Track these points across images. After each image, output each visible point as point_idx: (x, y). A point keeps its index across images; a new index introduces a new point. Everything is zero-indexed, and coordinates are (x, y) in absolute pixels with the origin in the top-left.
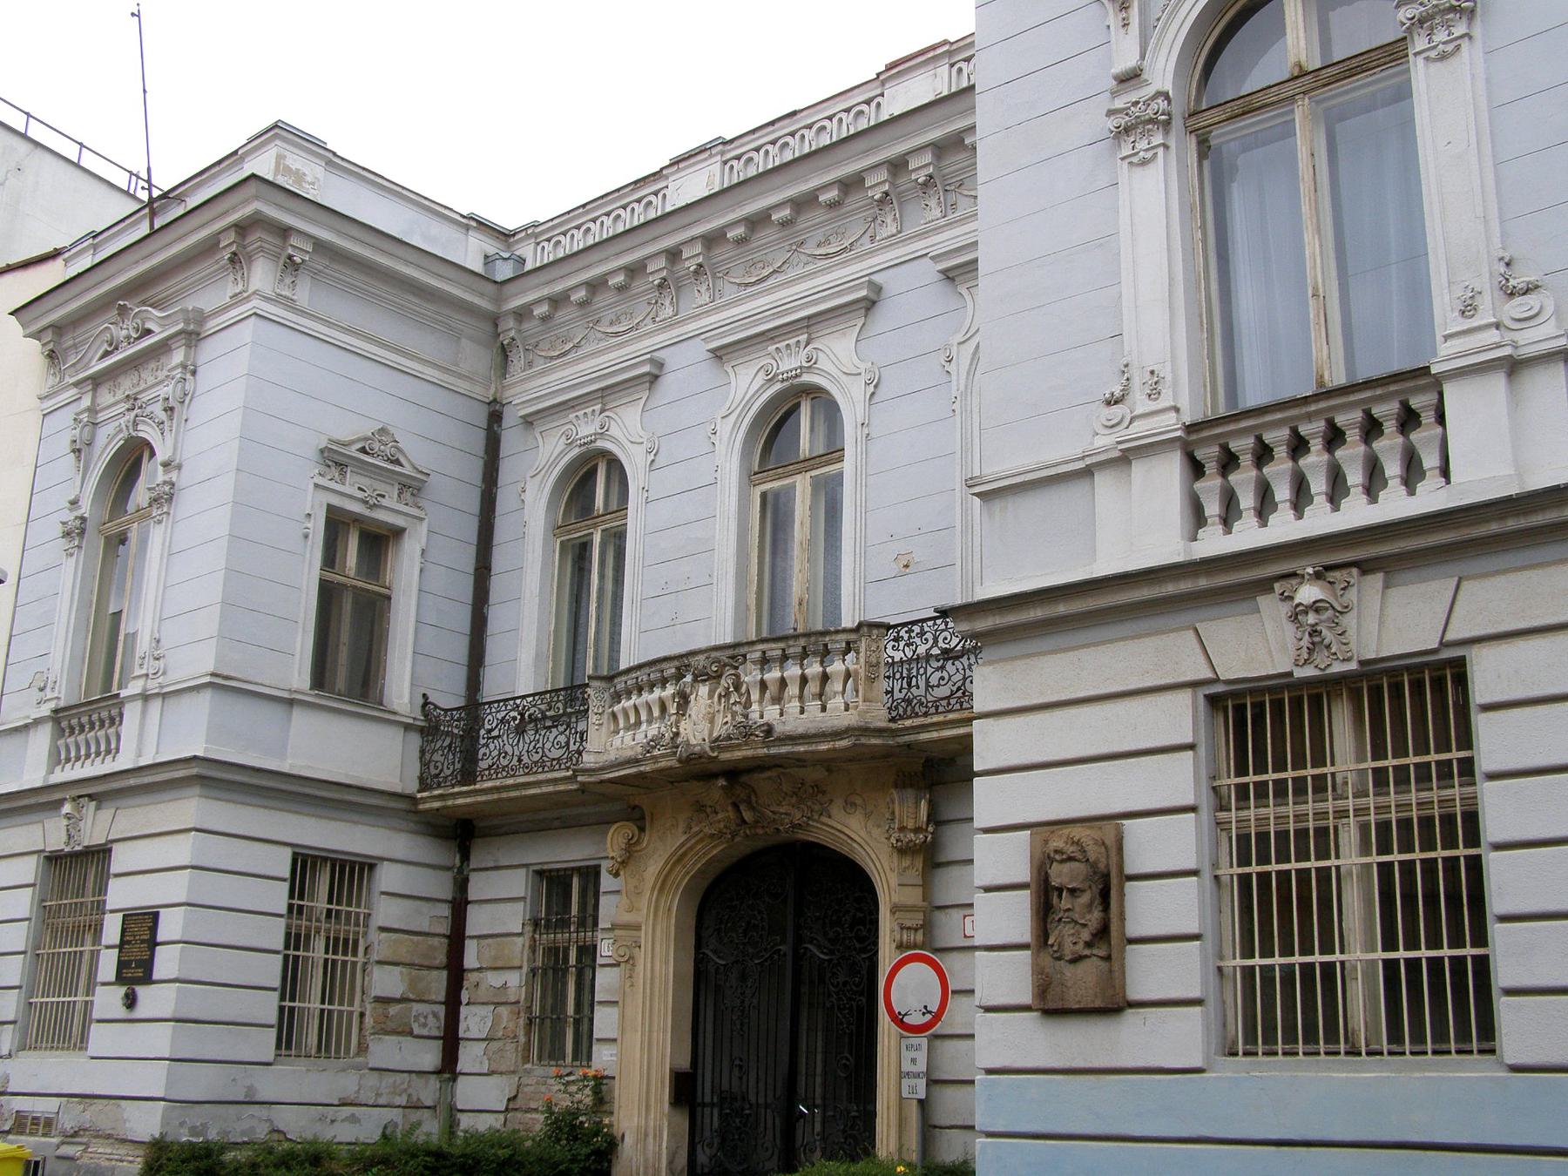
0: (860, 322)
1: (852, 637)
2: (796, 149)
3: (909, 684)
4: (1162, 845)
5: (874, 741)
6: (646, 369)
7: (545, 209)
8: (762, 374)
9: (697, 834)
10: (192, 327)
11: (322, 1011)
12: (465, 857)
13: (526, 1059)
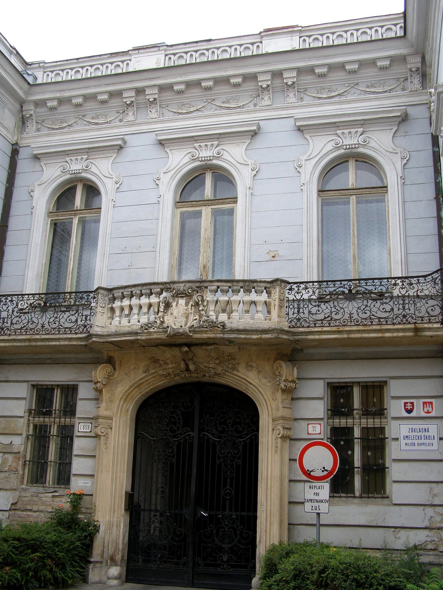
0: (248, 141)
1: (268, 285)
2: (209, 56)
5: (285, 337)
6: (120, 142)
7: (49, 58)
9: (153, 373)
13: (22, 483)
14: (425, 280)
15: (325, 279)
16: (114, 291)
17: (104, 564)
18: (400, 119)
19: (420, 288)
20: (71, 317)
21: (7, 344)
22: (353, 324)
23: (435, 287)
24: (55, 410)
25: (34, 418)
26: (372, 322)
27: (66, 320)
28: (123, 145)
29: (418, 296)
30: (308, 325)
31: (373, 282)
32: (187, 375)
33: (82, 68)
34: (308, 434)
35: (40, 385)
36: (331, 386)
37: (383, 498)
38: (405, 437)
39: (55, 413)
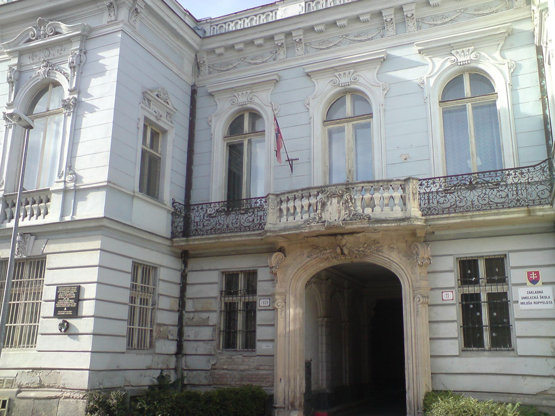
0: (378, 67)
4: (90, 292)
6: (275, 77)
7: (214, 15)
8: (332, 83)
10: (85, 33)
11: (139, 329)
14: (535, 169)
15: (449, 175)
16: (281, 196)
19: (530, 176)
21: (201, 242)
24: (241, 290)
26: (490, 207)
28: (278, 79)
29: (529, 183)
30: (437, 212)
31: (490, 174)
33: (240, 19)
37: (508, 350)
38: (524, 299)
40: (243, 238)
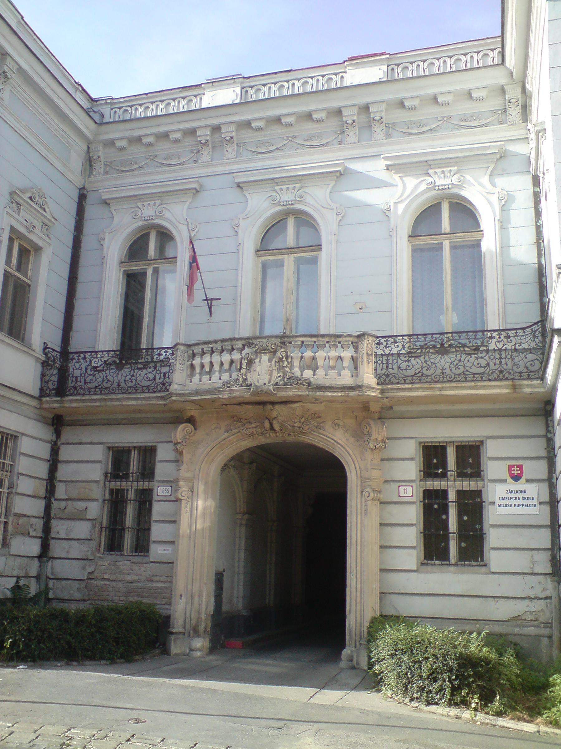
0: (333, 183)
3: (164, 376)
6: (195, 186)
12: (58, 434)
14: (524, 332)
17: (187, 635)
18: (498, 156)
19: (518, 341)
20: (149, 375)
22: (445, 380)
23: (534, 341)
24: (133, 473)
25: (110, 481)
26: (466, 378)
27: (143, 378)
29: (516, 350)
30: (397, 381)
31: (467, 335)
32: (271, 434)
34: (399, 496)
35: (116, 447)
36: (423, 446)
39: (133, 476)
40: (139, 402)
